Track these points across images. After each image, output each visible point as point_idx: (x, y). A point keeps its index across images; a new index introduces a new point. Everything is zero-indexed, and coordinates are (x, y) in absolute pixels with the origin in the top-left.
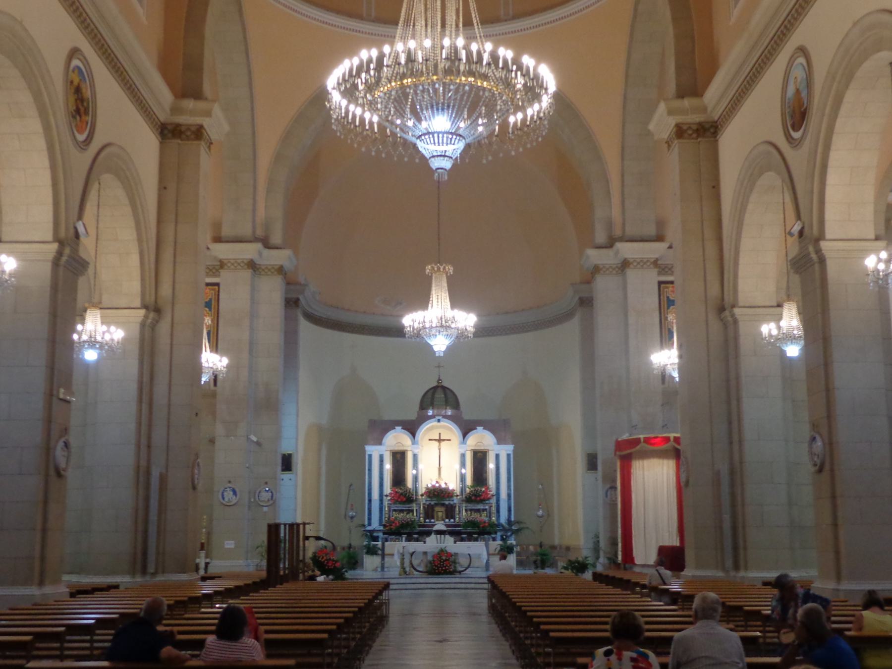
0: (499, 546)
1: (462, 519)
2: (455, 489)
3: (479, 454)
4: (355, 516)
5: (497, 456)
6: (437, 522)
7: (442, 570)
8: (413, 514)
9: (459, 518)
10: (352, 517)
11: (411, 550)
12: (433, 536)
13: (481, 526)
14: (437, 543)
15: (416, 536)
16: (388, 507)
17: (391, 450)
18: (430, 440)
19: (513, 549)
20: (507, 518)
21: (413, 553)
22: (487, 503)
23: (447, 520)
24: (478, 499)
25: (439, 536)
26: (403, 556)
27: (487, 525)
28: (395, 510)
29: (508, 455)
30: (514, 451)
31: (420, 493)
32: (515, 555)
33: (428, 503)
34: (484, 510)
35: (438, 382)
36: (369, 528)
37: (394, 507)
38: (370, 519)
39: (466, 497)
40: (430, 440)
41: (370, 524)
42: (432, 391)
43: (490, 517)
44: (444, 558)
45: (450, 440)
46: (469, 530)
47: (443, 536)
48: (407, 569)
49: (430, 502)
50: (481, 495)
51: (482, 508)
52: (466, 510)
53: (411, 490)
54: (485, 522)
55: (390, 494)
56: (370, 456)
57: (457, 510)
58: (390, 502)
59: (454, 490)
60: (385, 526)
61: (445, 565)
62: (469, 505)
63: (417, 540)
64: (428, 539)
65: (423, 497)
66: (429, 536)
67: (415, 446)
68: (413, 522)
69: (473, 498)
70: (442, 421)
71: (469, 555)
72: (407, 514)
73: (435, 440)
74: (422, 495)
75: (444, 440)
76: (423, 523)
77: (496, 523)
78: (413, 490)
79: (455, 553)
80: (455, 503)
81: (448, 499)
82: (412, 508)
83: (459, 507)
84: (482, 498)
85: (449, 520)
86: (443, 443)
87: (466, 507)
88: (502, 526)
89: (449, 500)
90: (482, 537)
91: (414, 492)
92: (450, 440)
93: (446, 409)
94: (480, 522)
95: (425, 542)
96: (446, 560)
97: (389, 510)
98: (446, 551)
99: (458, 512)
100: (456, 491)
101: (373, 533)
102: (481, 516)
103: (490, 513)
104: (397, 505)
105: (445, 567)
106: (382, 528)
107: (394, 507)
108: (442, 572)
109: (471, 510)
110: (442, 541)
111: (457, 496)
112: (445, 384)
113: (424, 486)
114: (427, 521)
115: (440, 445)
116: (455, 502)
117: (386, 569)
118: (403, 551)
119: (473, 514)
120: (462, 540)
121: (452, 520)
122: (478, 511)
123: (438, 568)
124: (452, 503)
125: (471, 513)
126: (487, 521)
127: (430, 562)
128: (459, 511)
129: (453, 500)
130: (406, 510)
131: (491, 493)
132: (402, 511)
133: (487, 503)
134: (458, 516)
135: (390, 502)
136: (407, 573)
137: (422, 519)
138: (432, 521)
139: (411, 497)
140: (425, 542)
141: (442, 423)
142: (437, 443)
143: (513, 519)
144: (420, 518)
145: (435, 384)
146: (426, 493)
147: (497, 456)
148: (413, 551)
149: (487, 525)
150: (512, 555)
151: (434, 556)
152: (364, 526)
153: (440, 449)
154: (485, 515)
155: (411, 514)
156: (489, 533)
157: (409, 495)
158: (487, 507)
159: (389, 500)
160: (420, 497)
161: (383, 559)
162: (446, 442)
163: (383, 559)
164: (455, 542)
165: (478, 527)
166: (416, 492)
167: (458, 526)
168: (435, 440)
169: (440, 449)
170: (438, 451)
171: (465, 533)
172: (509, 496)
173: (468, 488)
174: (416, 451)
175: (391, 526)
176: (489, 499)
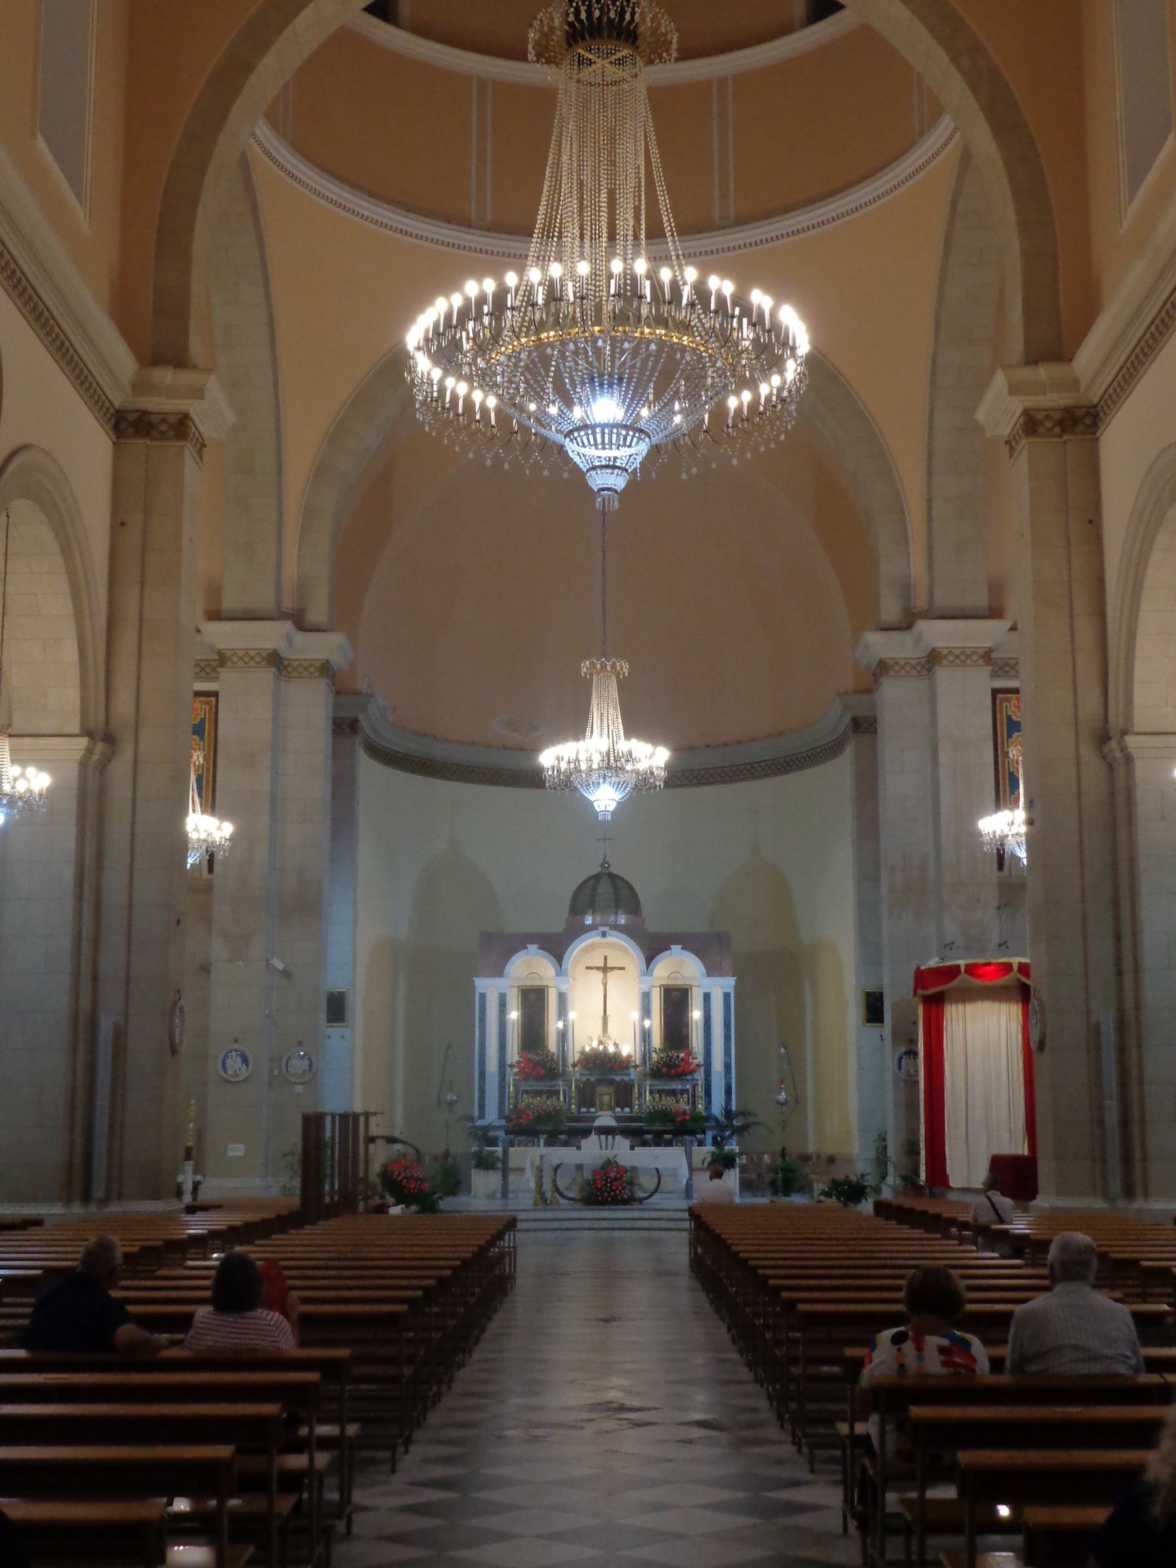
0: (710, 1155)
1: (644, 1107)
2: (633, 1054)
3: (674, 994)
4: (456, 1102)
5: (707, 997)
6: (599, 1113)
7: (609, 1196)
8: (558, 1099)
9: (640, 1106)
10: (451, 1104)
11: (556, 1162)
12: (593, 1137)
13: (679, 1119)
14: (601, 1149)
15: (563, 1137)
16: (514, 1085)
17: (519, 987)
18: (588, 968)
19: (735, 1160)
20: (724, 1105)
21: (559, 1166)
22: (688, 1080)
23: (618, 1110)
24: (673, 1071)
25: (603, 1137)
26: (541, 1171)
27: (687, 1118)
28: (527, 1092)
29: (727, 996)
30: (736, 988)
31: (570, 1061)
32: (738, 1169)
33: (584, 1079)
34: (683, 1092)
35: (602, 866)
36: (480, 1123)
37: (525, 1086)
38: (482, 1107)
39: (651, 1069)
40: (588, 968)
41: (482, 1116)
42: (591, 882)
43: (694, 1104)
44: (612, 1175)
45: (623, 969)
46: (658, 1127)
47: (610, 1137)
48: (549, 1195)
49: (587, 1077)
50: (677, 1066)
51: (680, 1087)
52: (651, 1092)
53: (555, 1057)
54: (685, 1113)
55: (518, 1062)
56: (483, 996)
57: (636, 1091)
58: (517, 1077)
59: (631, 1057)
60: (508, 1119)
61: (614, 1188)
62: (657, 1083)
63: (566, 1144)
64: (584, 1143)
65: (576, 1069)
66: (587, 1137)
67: (561, 978)
68: (558, 1112)
69: (664, 1069)
70: (610, 936)
71: (657, 1169)
72: (548, 1098)
73: (598, 968)
74: (574, 1065)
75: (613, 969)
76: (576, 1114)
77: (704, 1114)
78: (558, 1056)
79: (631, 1167)
80: (633, 1080)
81: (619, 1072)
82: (557, 1088)
83: (639, 1085)
84: (679, 1070)
85: (622, 1109)
86: (610, 974)
87: (650, 1086)
88: (716, 1120)
89: (622, 1075)
90: (680, 1138)
91: (560, 1059)
92: (623, 969)
93: (616, 913)
94: (676, 1112)
95: (579, 1148)
96: (616, 1179)
97: (516, 1092)
98: (616, 1162)
99: (637, 1095)
100: (633, 1058)
101: (488, 1131)
102: (678, 1102)
103: (694, 1096)
104: (530, 1083)
105: (615, 1191)
106: (503, 1122)
107: (525, 1086)
108: (609, 1199)
109: (660, 1092)
110: (610, 1147)
111: (636, 1066)
112: (614, 870)
113: (578, 1048)
114: (584, 1110)
115: (605, 976)
116: (632, 1077)
117: (510, 1195)
118: (541, 1162)
119: (664, 1098)
120: (645, 1144)
121: (627, 1109)
122: (673, 1093)
123: (602, 1192)
124: (626, 1078)
125: (661, 1097)
126: (688, 1112)
127: (588, 1183)
128: (640, 1094)
129: (629, 1075)
130: (548, 1091)
131: (697, 1061)
132: (538, 1093)
133: (688, 1080)
134: (637, 1102)
135: (517, 1077)
136: (548, 1202)
137: (573, 1106)
138: (593, 1110)
139: (555, 1069)
140: (579, 1148)
141: (609, 939)
142: (600, 975)
143: (734, 1108)
144: (570, 1105)
145: (595, 870)
146: (580, 1061)
147: (707, 997)
148: (559, 1162)
149: (687, 1118)
150: (732, 1171)
151: (595, 1172)
152: (472, 1119)
153: (605, 985)
154: (686, 1100)
155: (554, 1099)
156: (693, 1133)
157: (551, 1065)
158: (688, 1087)
159: (516, 1074)
160: (571, 1069)
161: (505, 1177)
162: (615, 972)
163: (505, 1177)
164: (632, 1148)
165: (673, 1121)
166: (564, 1060)
167: (638, 1119)
168: (598, 968)
169: (605, 985)
170: (602, 988)
171: (648, 1132)
172: (727, 1067)
173: (655, 1051)
174: (563, 988)
175: (520, 1118)
176: (692, 1072)
